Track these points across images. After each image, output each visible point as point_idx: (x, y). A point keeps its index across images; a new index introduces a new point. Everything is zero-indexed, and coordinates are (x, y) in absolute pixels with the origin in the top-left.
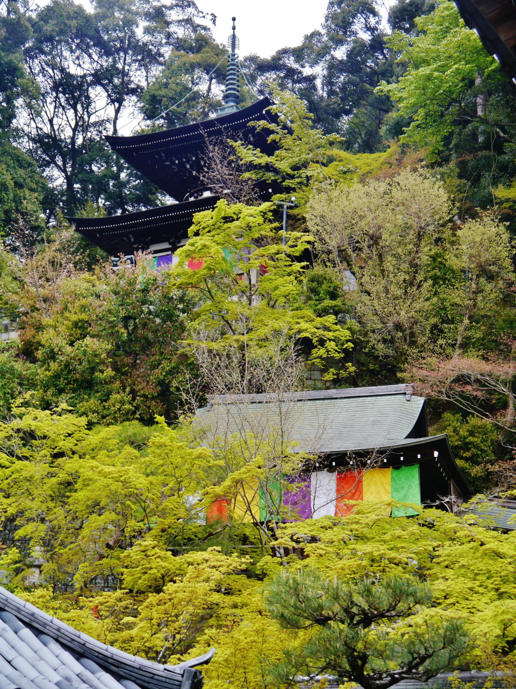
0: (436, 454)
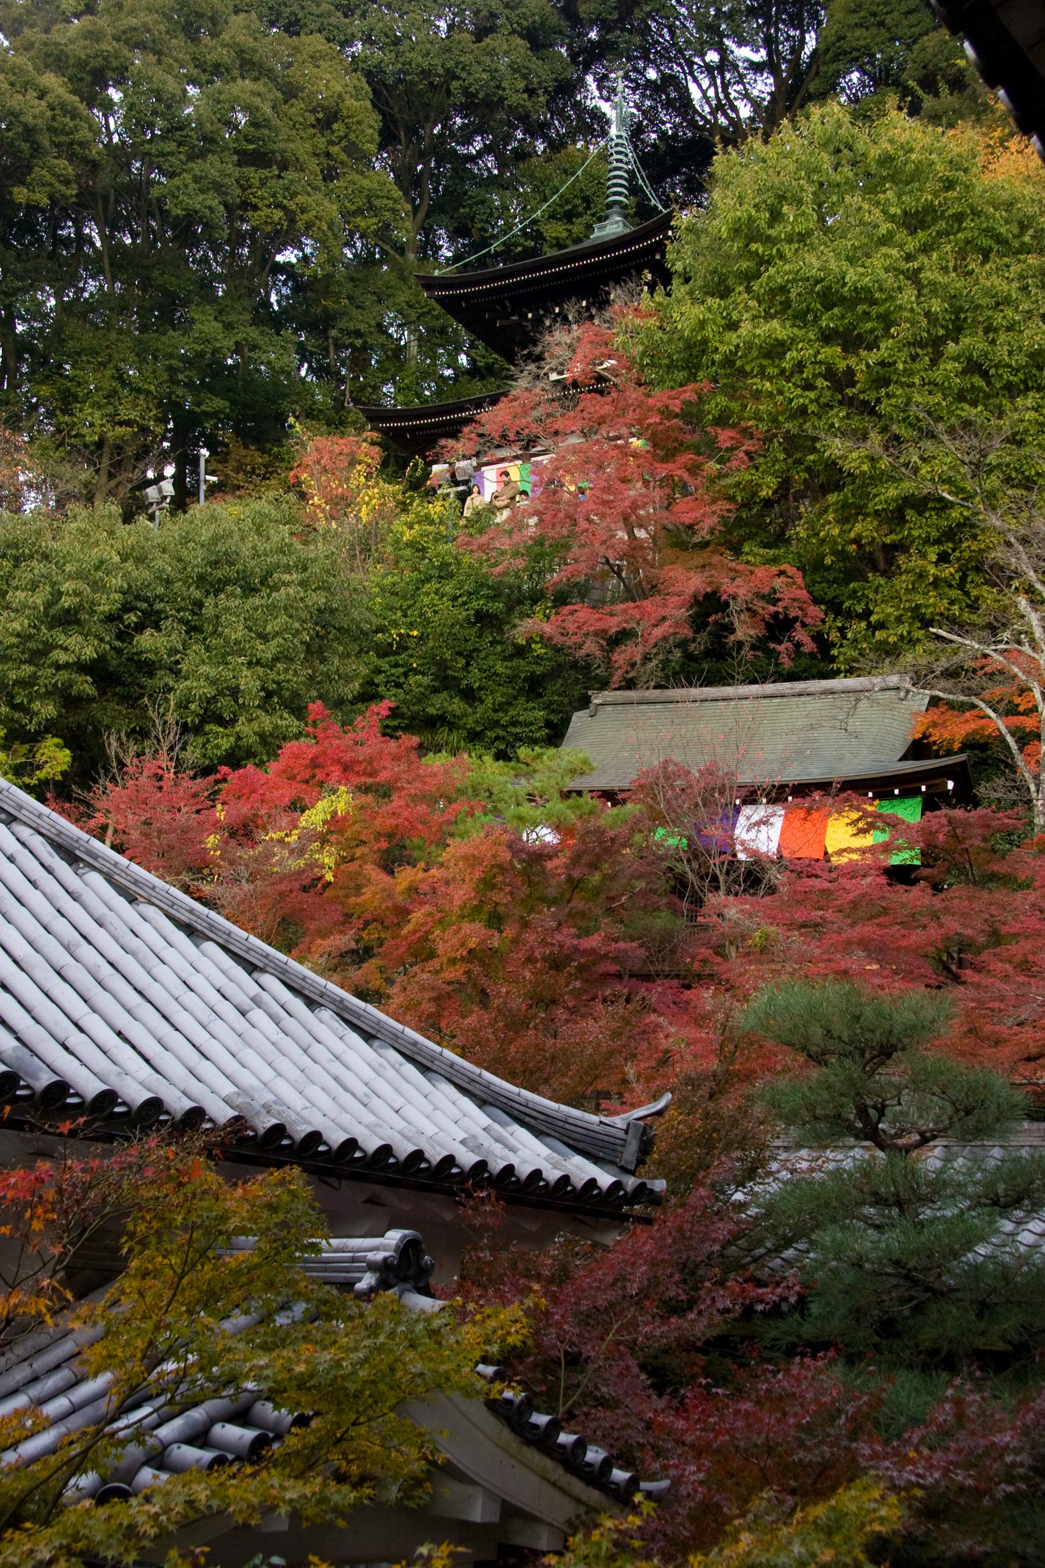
0: (950, 785)
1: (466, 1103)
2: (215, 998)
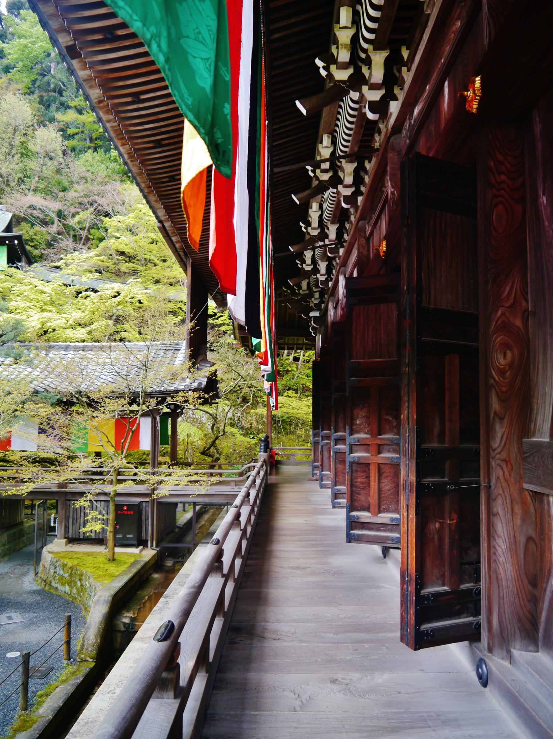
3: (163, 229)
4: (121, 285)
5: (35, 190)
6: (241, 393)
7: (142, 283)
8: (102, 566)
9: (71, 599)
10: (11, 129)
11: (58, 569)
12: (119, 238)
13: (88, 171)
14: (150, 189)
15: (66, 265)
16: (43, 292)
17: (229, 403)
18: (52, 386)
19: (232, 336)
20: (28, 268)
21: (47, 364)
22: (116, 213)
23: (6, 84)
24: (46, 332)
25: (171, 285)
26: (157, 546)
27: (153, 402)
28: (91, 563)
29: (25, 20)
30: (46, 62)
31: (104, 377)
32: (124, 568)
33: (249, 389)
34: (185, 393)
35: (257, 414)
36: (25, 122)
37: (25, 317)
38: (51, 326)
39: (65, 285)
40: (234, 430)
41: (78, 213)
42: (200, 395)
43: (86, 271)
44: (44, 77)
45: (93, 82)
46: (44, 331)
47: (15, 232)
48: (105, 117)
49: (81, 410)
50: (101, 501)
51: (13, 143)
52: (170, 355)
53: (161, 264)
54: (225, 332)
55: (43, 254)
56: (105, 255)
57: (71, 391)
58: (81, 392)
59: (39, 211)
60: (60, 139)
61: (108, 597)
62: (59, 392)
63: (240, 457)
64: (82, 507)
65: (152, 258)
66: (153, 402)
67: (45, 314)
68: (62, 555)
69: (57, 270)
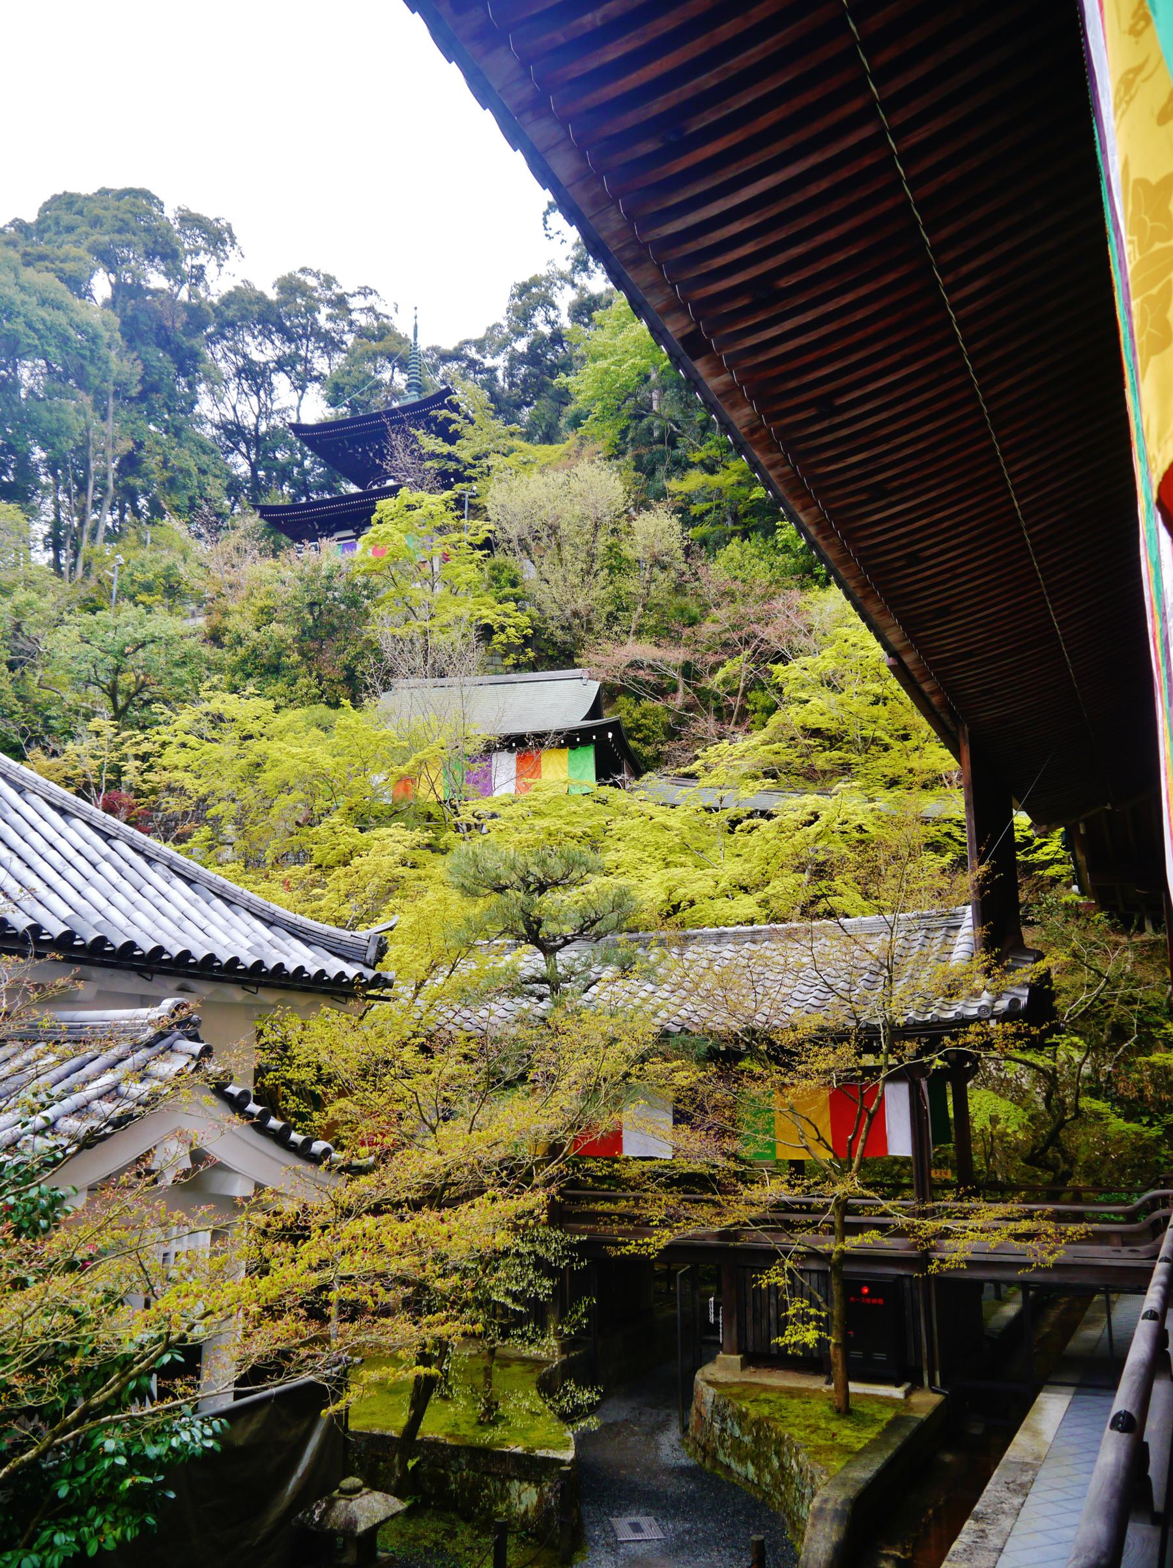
0: (610, 735)
1: (257, 924)
2: (71, 854)
3: (900, 670)
4: (820, 797)
5: (639, 633)
6: (1108, 1016)
7: (861, 789)
8: (823, 1425)
9: (759, 1497)
10: (589, 526)
11: (730, 1424)
12: (807, 701)
13: (736, 578)
14: (869, 589)
15: (707, 769)
16: (667, 828)
17: (1081, 1043)
18: (696, 1019)
19: (1075, 888)
20: (635, 784)
21: (682, 974)
22: (797, 653)
23: (575, 449)
24: (676, 908)
25: (925, 787)
26: (943, 1385)
27: (911, 1047)
28: (797, 1416)
29: (602, 327)
30: (644, 391)
31: (800, 997)
32: (871, 1434)
33: (1126, 1008)
34: (983, 1026)
35: (1152, 1065)
36: (613, 508)
37: (634, 881)
38: (685, 895)
39: (708, 809)
40: (1099, 1105)
41: (721, 664)
42: (1019, 1028)
43: (745, 776)
44: (640, 421)
45: (739, 395)
46: (673, 906)
47: (608, 717)
48: (763, 459)
49: (758, 1069)
50: (810, 1271)
51: (594, 551)
52: (940, 940)
53: (897, 745)
54: (1055, 881)
55: (660, 753)
56: (780, 741)
57: (734, 1029)
58: (754, 1032)
59: (647, 671)
60: (678, 528)
61: (844, 1503)
62: (711, 1033)
63: (1122, 1171)
64: (773, 1289)
65: (878, 734)
66: (911, 1047)
67: (674, 871)
68: (735, 1390)
69: (690, 782)
